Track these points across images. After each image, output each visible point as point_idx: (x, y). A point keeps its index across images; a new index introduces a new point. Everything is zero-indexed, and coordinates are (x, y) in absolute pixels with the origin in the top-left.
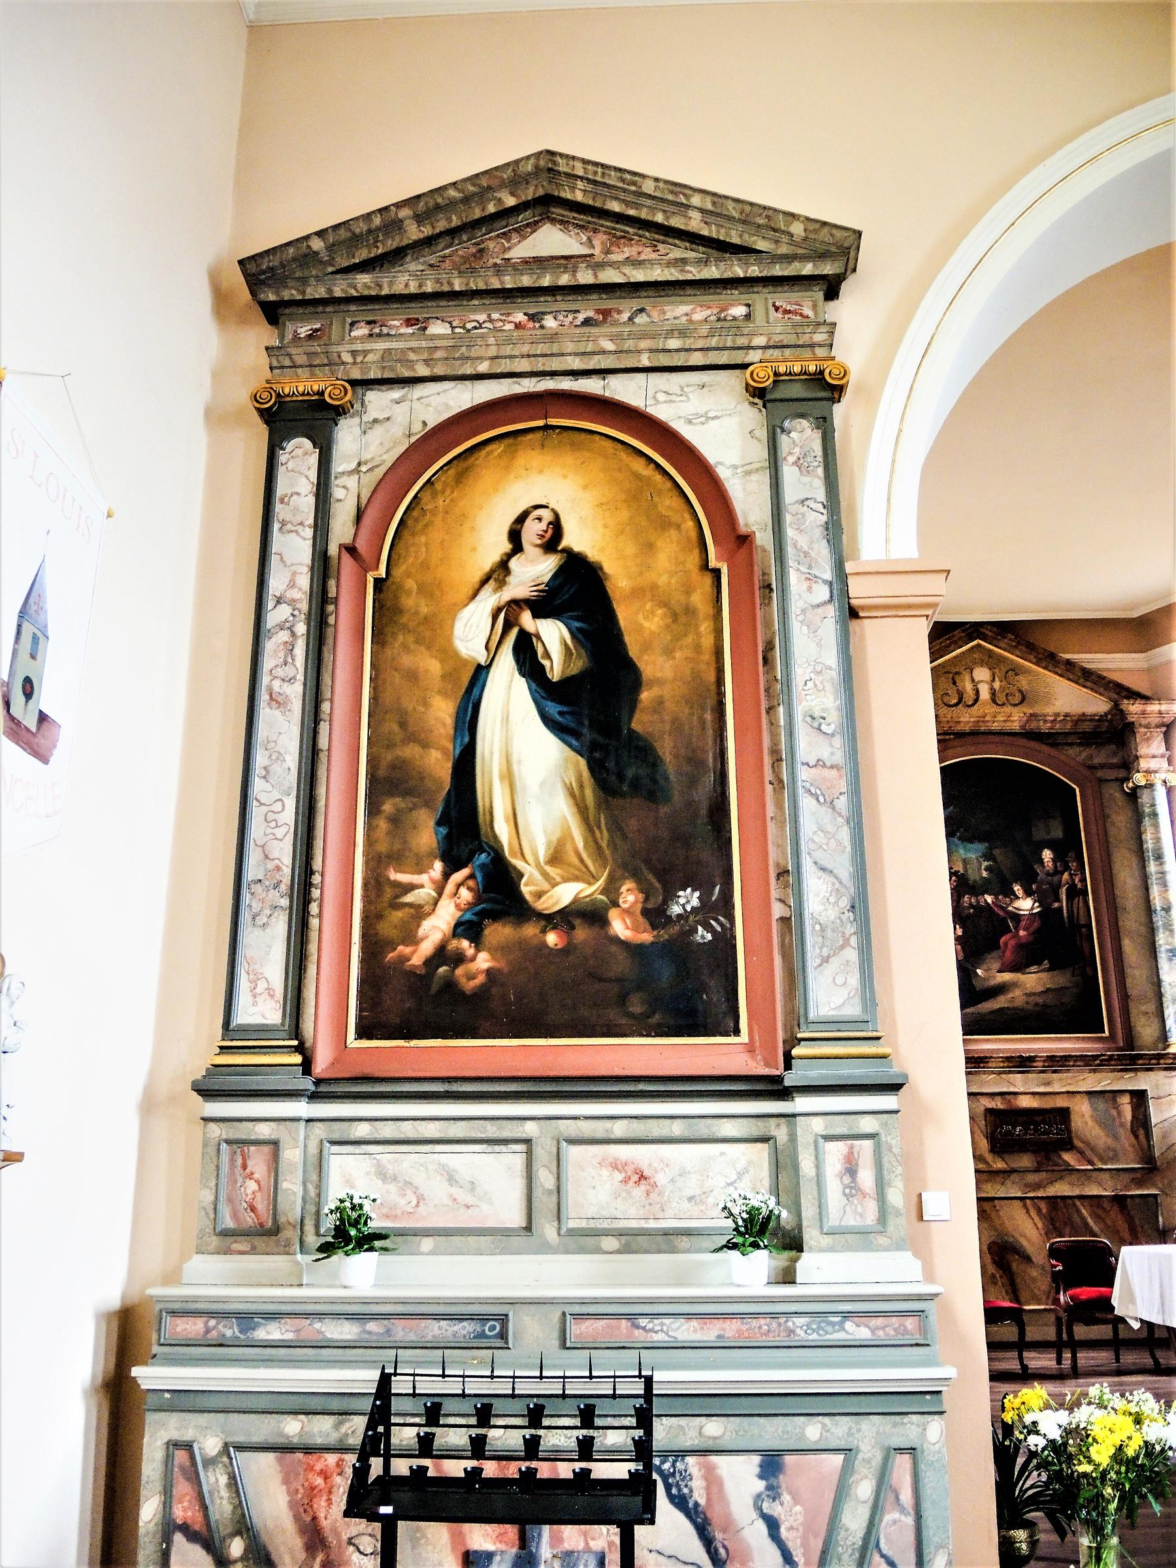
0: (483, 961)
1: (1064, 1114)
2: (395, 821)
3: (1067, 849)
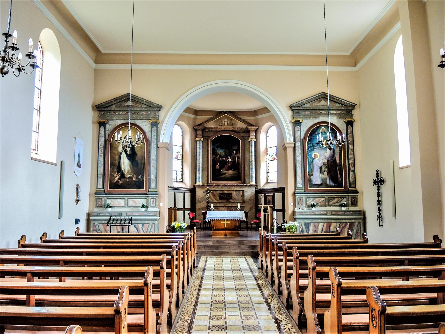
0: (121, 182)
1: (231, 194)
2: (113, 168)
3: (238, 151)
